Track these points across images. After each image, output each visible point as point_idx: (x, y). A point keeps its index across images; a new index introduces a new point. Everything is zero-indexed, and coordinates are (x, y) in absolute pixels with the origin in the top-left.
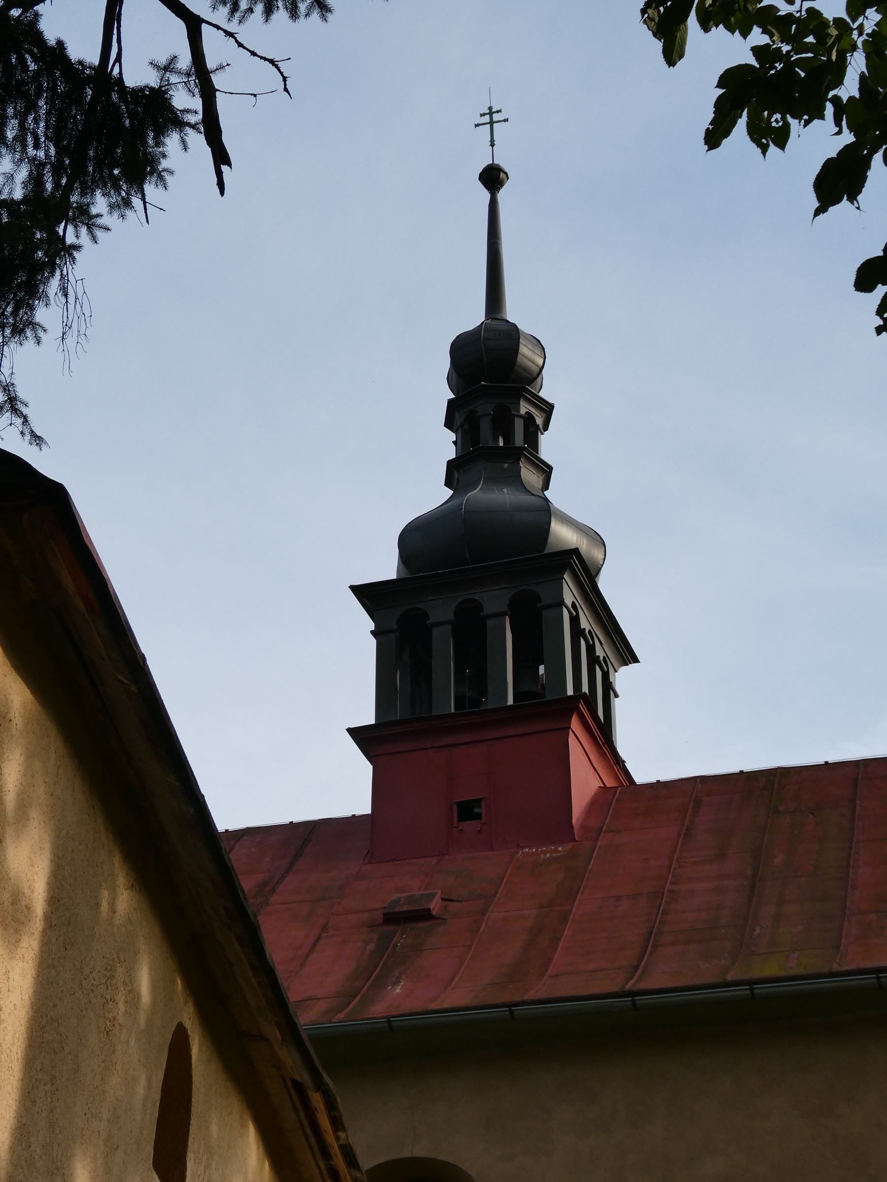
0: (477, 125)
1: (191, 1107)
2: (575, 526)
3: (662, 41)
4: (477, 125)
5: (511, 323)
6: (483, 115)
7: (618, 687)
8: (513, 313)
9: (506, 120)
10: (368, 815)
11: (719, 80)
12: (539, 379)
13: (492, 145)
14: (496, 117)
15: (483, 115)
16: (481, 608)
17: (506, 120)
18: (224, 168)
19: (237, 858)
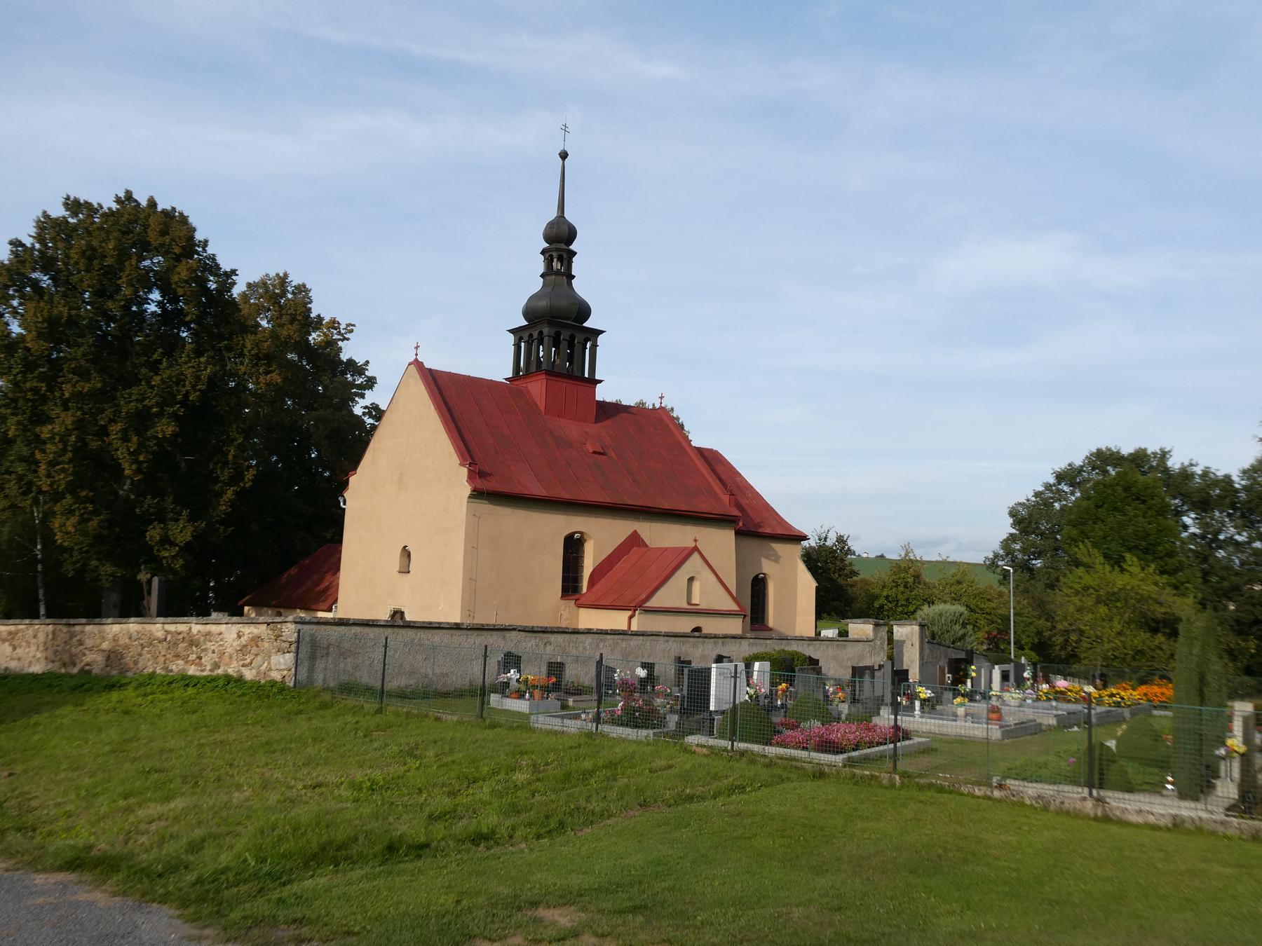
8: (568, 216)
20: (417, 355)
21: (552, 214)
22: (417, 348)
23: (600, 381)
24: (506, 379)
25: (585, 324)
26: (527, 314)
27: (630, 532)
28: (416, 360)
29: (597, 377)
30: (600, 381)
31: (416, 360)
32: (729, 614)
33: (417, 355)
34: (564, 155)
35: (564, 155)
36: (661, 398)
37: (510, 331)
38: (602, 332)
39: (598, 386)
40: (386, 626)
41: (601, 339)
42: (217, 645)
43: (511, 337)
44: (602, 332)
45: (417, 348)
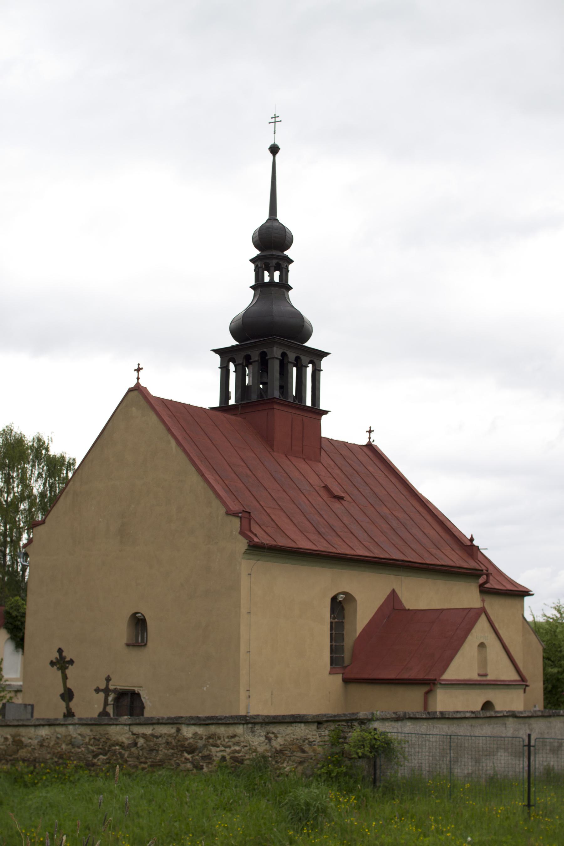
0: (270, 123)
1: (302, 386)
2: (286, 513)
3: (67, 665)
4: (270, 123)
5: (280, 223)
6: (272, 118)
7: (68, 676)
8: (282, 217)
9: (280, 121)
10: (306, 404)
11: (152, 395)
12: (286, 228)
13: (275, 133)
14: (277, 119)
15: (272, 118)
16: (269, 264)
17: (280, 121)
18: (323, 485)
19: (322, 439)
20: (138, 378)
21: (263, 217)
22: (138, 370)
23: (326, 412)
24: (209, 408)
25: (307, 344)
26: (235, 332)
27: (388, 591)
28: (138, 385)
29: (322, 407)
30: (326, 412)
31: (138, 385)
32: (480, 684)
33: (138, 378)
34: (274, 150)
35: (274, 150)
36: (370, 432)
37: (216, 351)
38: (326, 354)
39: (324, 418)
40: (475, 716)
41: (325, 363)
42: (228, 750)
43: (217, 359)
44: (326, 354)
45: (138, 370)
